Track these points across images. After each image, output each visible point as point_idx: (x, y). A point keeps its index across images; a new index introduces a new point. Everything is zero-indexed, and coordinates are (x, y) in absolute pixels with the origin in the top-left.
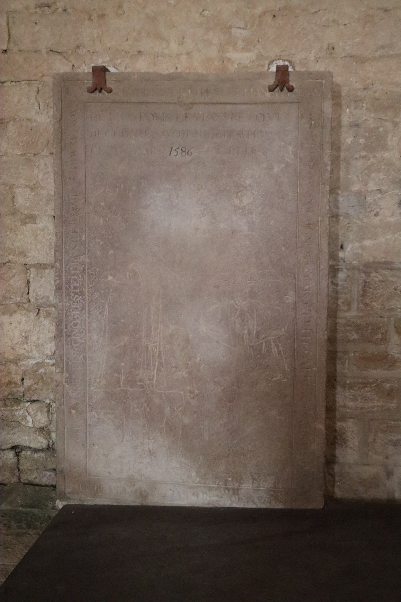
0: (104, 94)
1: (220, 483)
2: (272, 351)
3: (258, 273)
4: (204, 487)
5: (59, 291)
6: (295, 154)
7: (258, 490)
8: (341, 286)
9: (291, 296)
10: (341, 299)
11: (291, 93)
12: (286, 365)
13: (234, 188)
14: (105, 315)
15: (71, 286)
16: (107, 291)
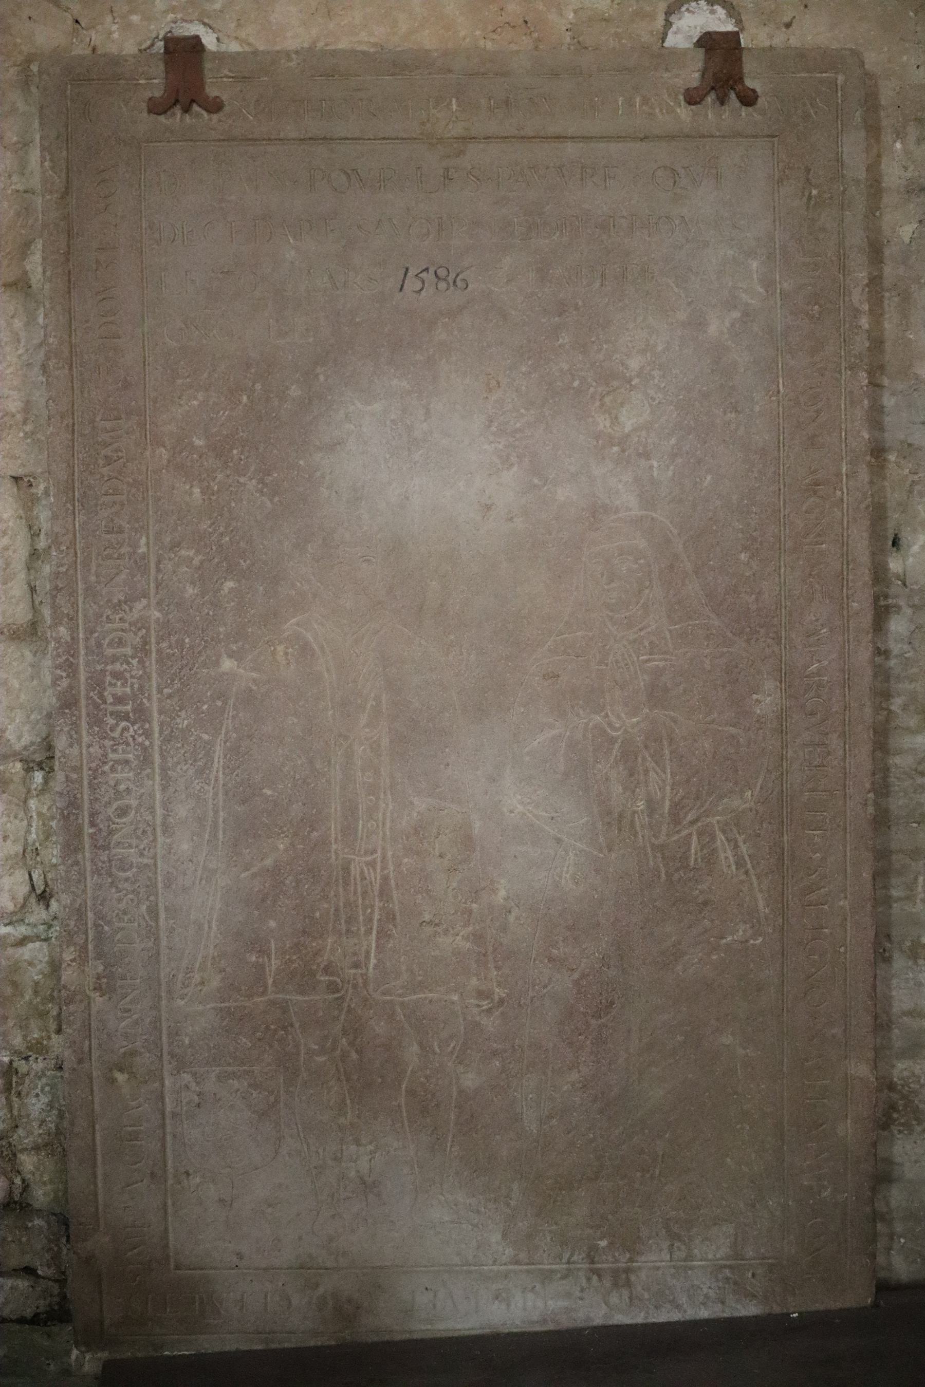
0: (198, 115)
1: (575, 1258)
2: (717, 857)
3: (670, 631)
4: (528, 1271)
5: (67, 711)
6: (768, 284)
7: (686, 1268)
8: (896, 656)
9: (769, 695)
10: (899, 695)
11: (750, 109)
12: (759, 896)
13: (594, 384)
14: (212, 777)
15: (106, 694)
16: (219, 703)
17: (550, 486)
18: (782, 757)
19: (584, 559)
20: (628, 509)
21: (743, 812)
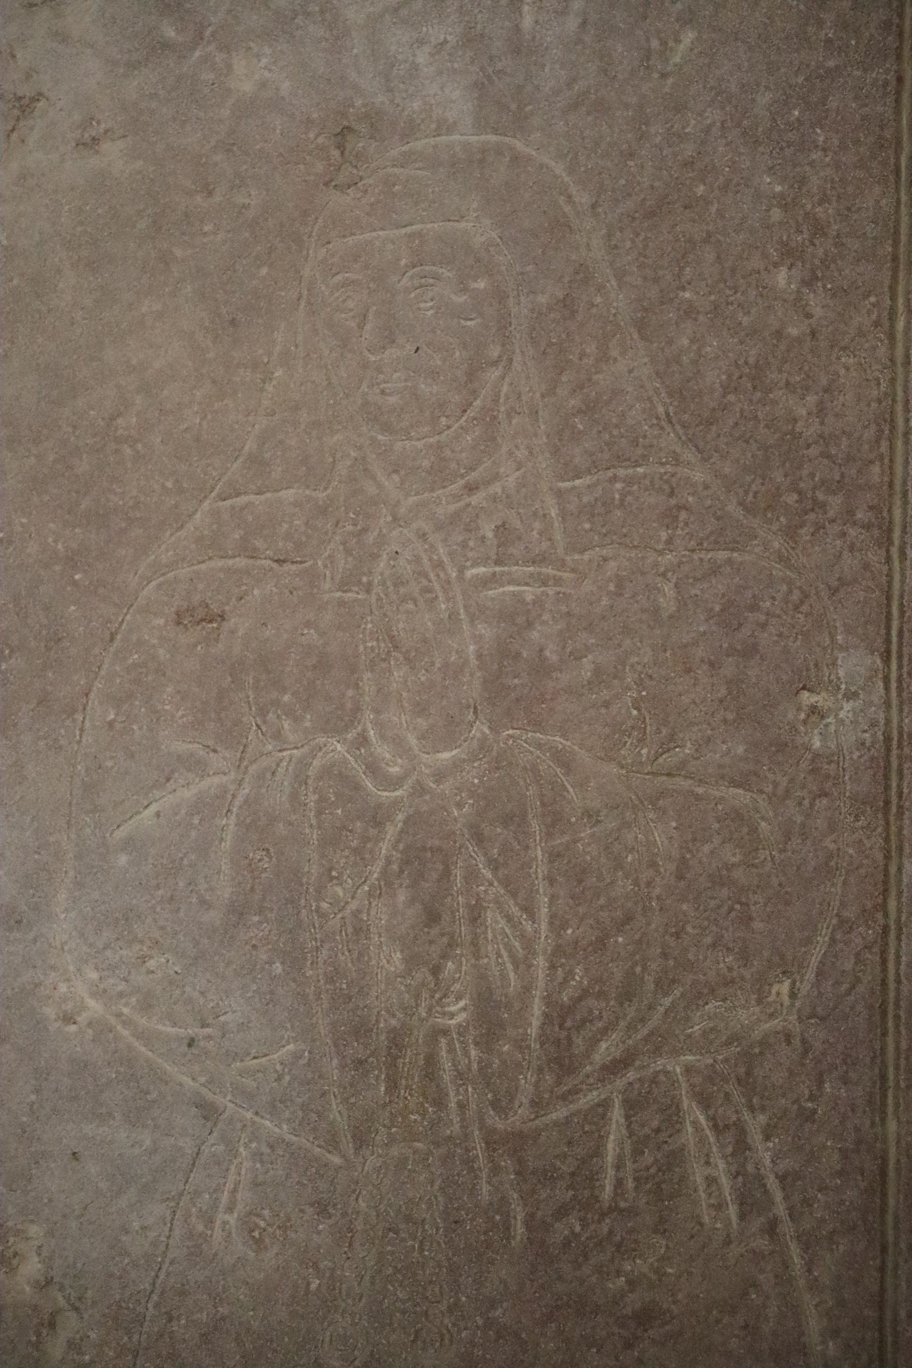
2: (683, 1179)
3: (559, 494)
9: (851, 696)
17: (211, 48)
18: (885, 882)
19: (306, 272)
20: (444, 127)
21: (764, 1043)
